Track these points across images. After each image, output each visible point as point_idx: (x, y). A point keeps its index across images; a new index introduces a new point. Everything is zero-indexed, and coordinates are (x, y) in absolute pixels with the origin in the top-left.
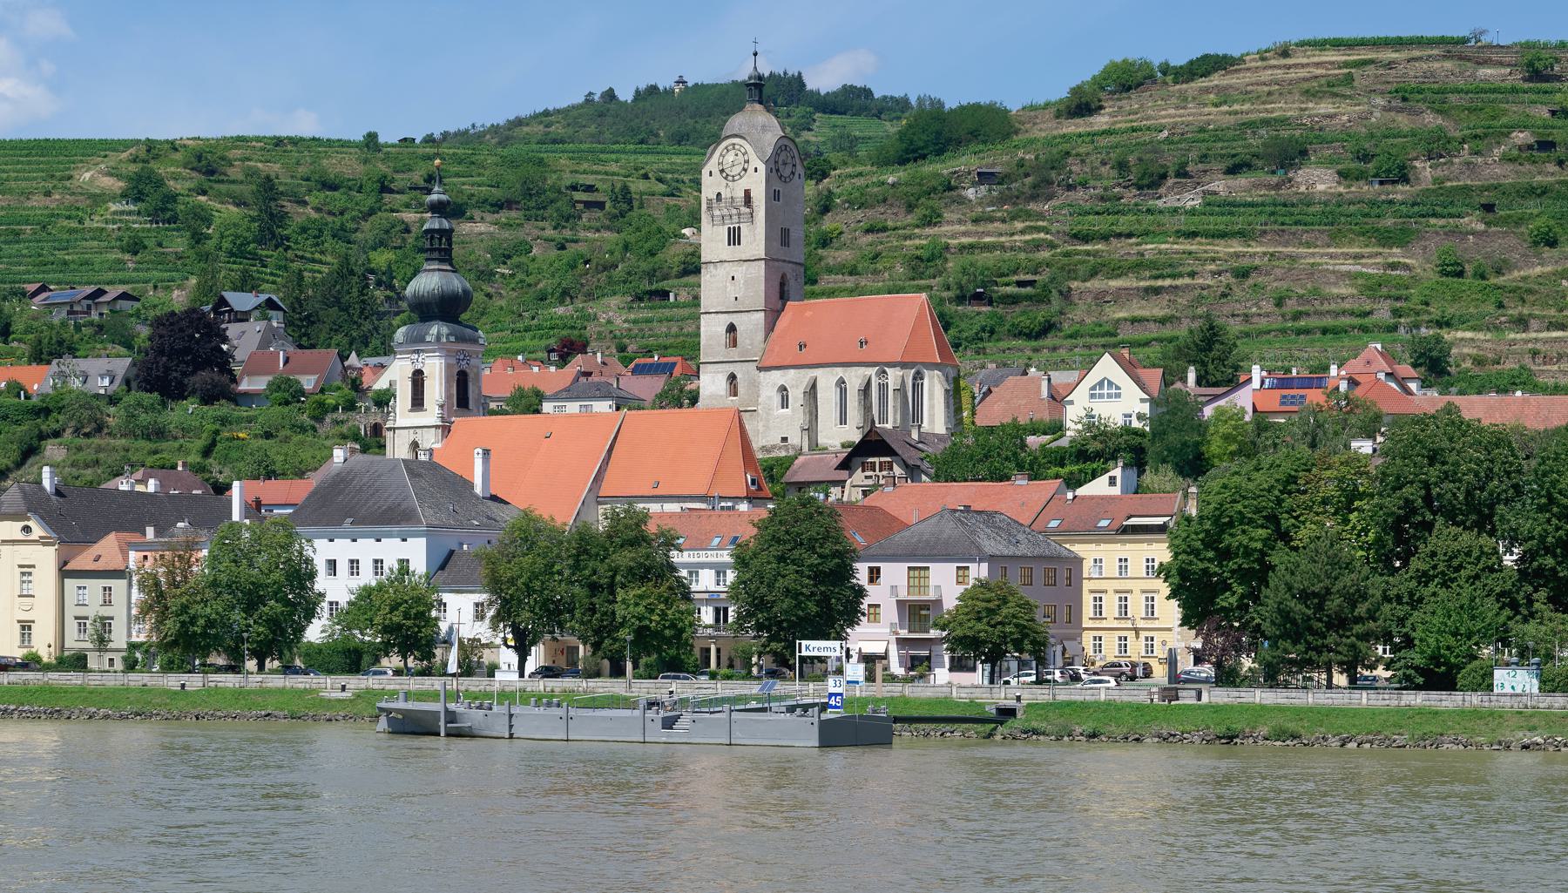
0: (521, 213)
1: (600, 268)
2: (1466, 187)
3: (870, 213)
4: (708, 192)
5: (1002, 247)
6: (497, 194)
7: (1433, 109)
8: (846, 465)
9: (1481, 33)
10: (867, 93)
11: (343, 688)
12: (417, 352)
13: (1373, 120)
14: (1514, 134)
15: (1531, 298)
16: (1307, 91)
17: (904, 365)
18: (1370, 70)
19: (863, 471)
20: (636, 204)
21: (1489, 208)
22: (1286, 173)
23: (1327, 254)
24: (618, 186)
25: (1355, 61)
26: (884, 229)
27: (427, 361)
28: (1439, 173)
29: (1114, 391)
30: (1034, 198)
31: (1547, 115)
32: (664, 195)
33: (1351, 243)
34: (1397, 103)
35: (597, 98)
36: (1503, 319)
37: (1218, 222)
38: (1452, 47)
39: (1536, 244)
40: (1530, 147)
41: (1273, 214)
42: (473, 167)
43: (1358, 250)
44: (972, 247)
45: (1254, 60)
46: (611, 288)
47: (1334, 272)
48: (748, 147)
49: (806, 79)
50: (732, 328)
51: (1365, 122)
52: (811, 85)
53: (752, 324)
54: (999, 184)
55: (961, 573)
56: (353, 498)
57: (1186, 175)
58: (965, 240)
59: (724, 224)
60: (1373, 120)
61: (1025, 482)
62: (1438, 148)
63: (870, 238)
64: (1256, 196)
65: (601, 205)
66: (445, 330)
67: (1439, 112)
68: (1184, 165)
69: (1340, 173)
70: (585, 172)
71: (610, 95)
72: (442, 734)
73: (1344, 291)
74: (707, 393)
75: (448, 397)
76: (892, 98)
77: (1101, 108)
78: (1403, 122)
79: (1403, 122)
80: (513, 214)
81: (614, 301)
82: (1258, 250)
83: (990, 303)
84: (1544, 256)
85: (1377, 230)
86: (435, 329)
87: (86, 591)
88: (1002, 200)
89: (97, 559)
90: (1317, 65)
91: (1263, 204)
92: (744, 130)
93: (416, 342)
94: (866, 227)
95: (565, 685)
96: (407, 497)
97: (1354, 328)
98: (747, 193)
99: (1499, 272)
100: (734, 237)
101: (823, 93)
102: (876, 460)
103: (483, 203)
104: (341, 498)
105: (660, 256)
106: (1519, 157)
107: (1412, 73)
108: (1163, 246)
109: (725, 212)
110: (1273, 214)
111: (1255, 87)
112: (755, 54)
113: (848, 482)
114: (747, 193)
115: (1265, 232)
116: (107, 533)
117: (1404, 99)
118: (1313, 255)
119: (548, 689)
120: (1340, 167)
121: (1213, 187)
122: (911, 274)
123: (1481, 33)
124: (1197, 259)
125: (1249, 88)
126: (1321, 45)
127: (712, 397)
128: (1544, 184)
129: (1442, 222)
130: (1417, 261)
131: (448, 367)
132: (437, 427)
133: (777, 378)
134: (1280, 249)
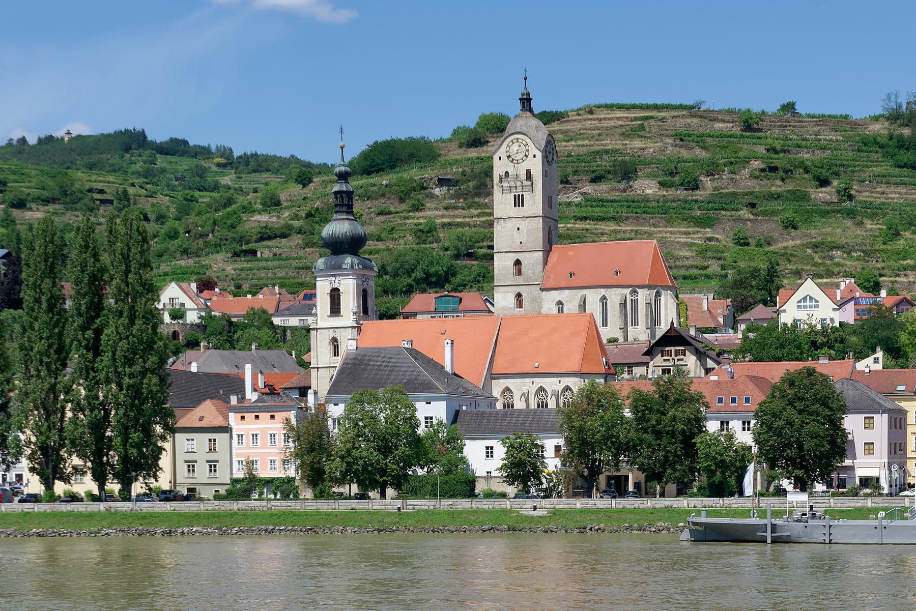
0: (62, 206)
1: (198, 236)
2: (734, 193)
3: (376, 203)
4: (498, 172)
5: (469, 224)
6: (45, 194)
7: (699, 146)
8: (650, 353)
9: (701, 103)
10: (185, 142)
11: (535, 508)
12: (335, 276)
13: (668, 152)
14: (751, 162)
15: (794, 259)
16: (623, 134)
17: (650, 287)
18: (652, 122)
19: (662, 356)
20: (132, 201)
21: (753, 205)
22: (628, 183)
23: (669, 232)
24: (121, 190)
25: (641, 117)
26: (390, 213)
27: (343, 282)
28: (715, 184)
29: (814, 303)
30: (477, 195)
31: (764, 152)
32: (146, 196)
33: (679, 224)
34: (678, 142)
35: (15, 143)
36: (787, 271)
37: (597, 211)
38: (692, 110)
39: (786, 227)
40: (763, 170)
41: (628, 207)
42: (24, 177)
43: (684, 229)
44: (450, 224)
45: (573, 115)
46: (217, 247)
47: (678, 242)
48: (528, 140)
49: (147, 134)
50: (518, 263)
51: (664, 153)
52: (150, 137)
53: (533, 260)
54: (453, 186)
55: (867, 421)
56: (376, 374)
57: (567, 182)
58: (446, 220)
59: (511, 192)
60: (668, 152)
61: (827, 362)
62: (712, 170)
63: (382, 218)
64: (615, 195)
65: (111, 202)
66: (356, 261)
67: (703, 148)
68: (566, 176)
69: (660, 183)
70: (96, 181)
71: (23, 141)
72: (769, 541)
73: (688, 254)
74: (500, 306)
75: (358, 307)
76: (199, 146)
77: (488, 142)
78: (685, 153)
79: (685, 153)
80: (57, 206)
81: (220, 257)
82: (628, 228)
83: (477, 259)
84: (793, 234)
85: (694, 218)
86: (348, 260)
87: (194, 442)
88: (458, 196)
89: (201, 419)
90: (618, 119)
91: (620, 201)
92: (524, 129)
93: (334, 269)
94: (378, 211)
95: (705, 502)
96: (419, 373)
97: (701, 276)
98: (528, 172)
99: (769, 244)
100: (519, 201)
101: (158, 142)
102: (673, 348)
103: (37, 199)
104: (366, 375)
105: (239, 228)
106: (760, 175)
107: (678, 125)
108: (569, 225)
109: (512, 184)
110: (628, 207)
111: (585, 131)
112: (525, 79)
113: (651, 363)
114: (528, 172)
115: (628, 218)
116: (204, 400)
117: (682, 140)
118: (660, 232)
119: (691, 506)
120: (659, 179)
121: (585, 189)
122: (417, 241)
123: (701, 103)
124: (592, 233)
125: (582, 131)
126: (611, 107)
127: (503, 309)
128: (778, 192)
129: (728, 213)
130: (722, 236)
131: (358, 285)
132: (353, 327)
133: (556, 295)
134: (640, 228)
